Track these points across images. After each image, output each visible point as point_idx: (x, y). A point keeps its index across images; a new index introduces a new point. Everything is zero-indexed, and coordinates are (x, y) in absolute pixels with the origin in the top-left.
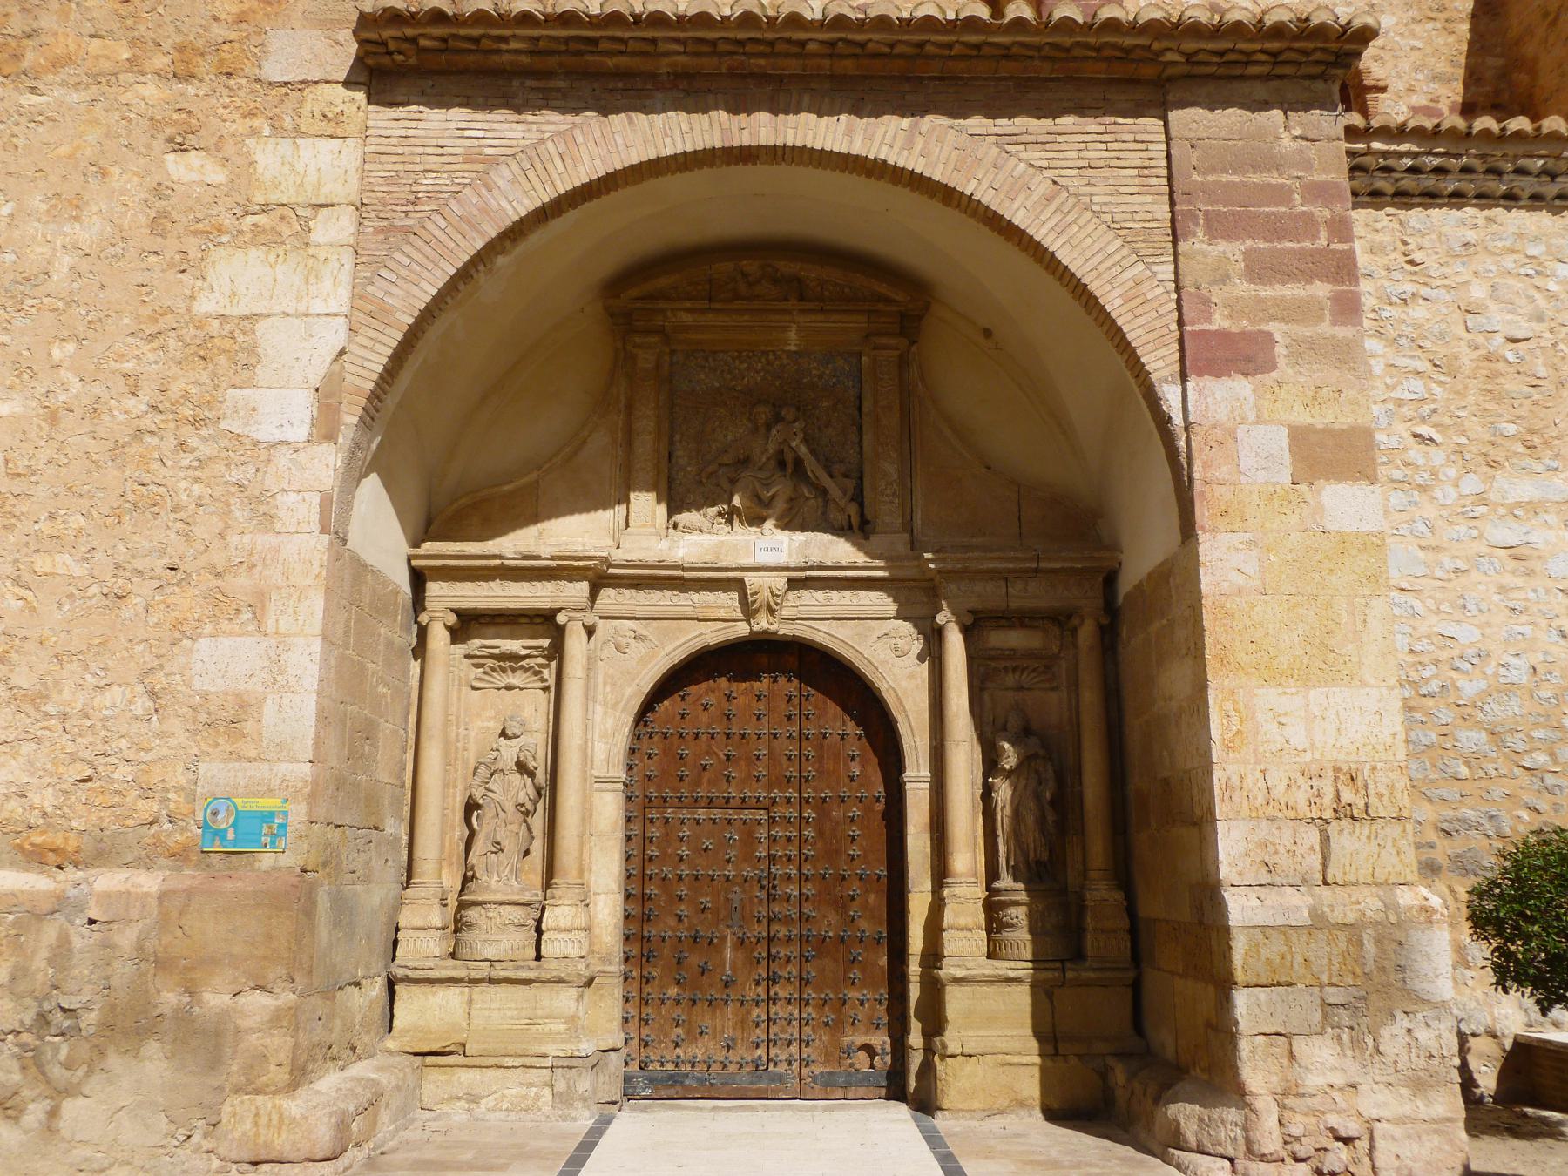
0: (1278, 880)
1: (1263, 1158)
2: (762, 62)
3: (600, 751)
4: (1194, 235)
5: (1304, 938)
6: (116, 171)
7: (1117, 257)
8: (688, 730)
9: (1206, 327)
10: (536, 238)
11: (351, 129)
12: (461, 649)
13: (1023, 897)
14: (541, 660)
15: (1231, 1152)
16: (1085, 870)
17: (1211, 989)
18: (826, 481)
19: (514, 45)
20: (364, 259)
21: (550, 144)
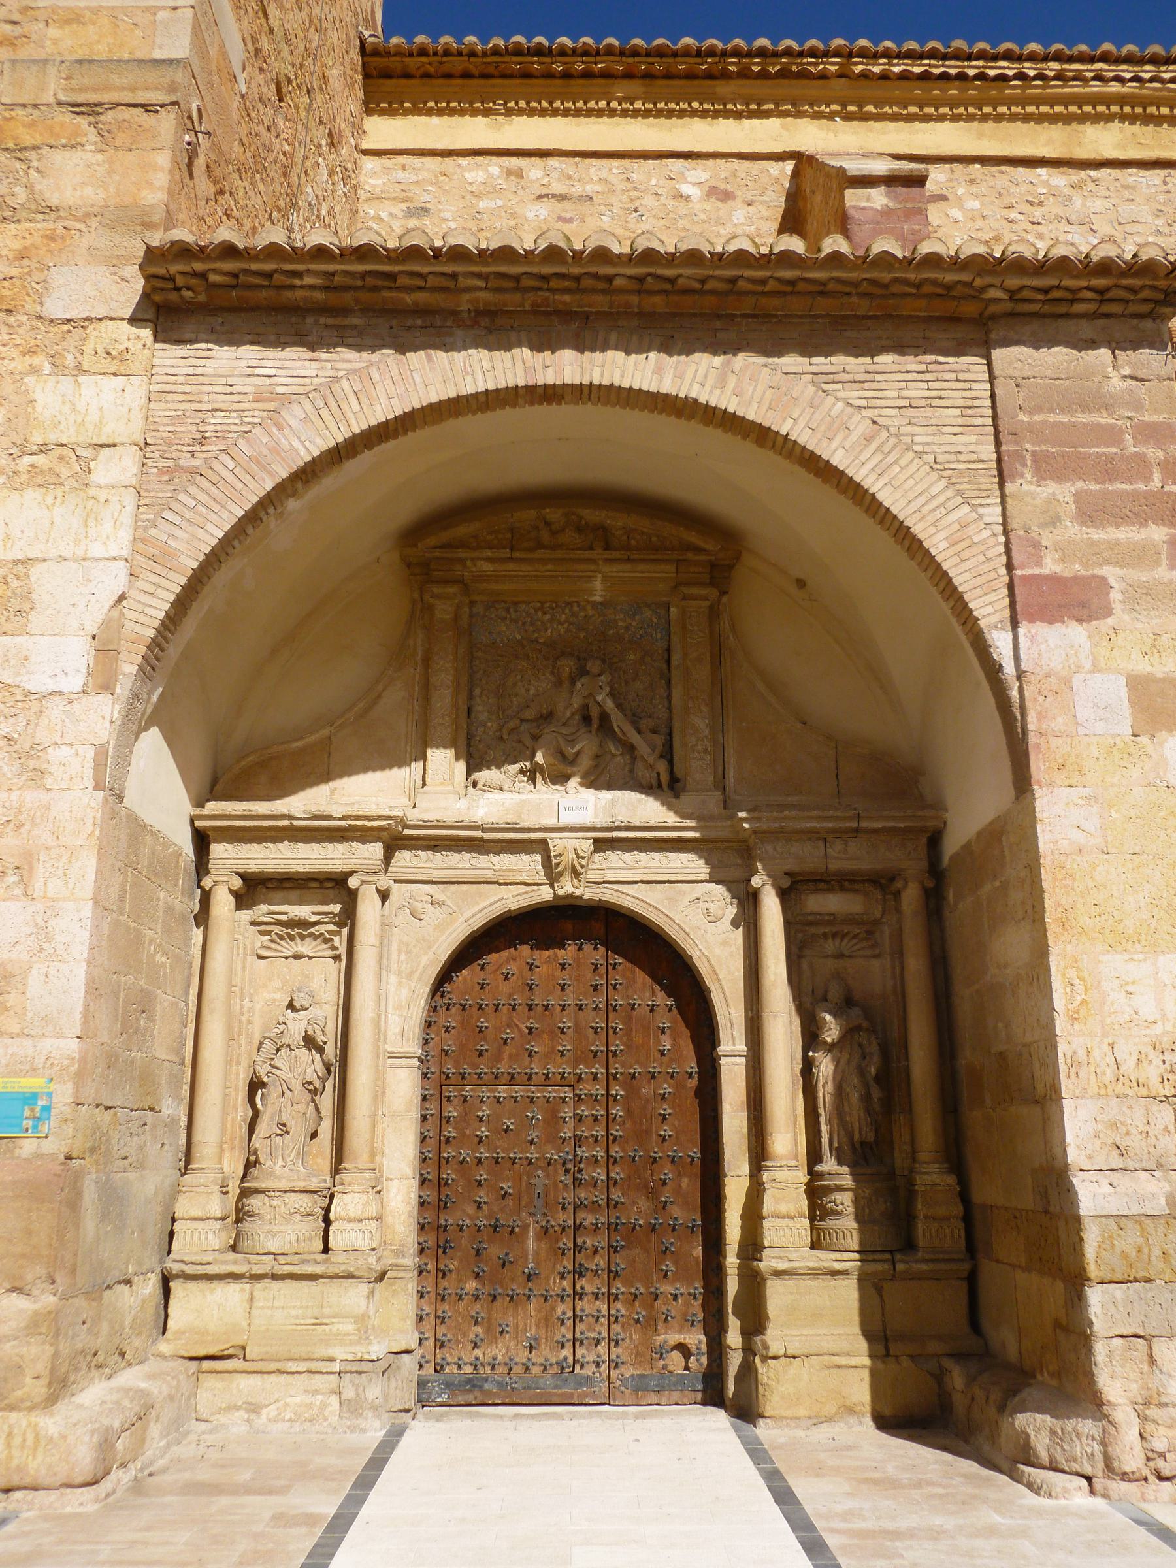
0: (1131, 1165)
1: (1124, 1476)
2: (567, 298)
3: (394, 1024)
4: (1022, 476)
5: (1162, 1229)
7: (941, 499)
8: (487, 1000)
9: (1037, 571)
10: (329, 482)
11: (137, 366)
12: (246, 915)
13: (848, 1181)
14: (331, 927)
15: (1088, 1470)
16: (914, 1152)
17: (1060, 1285)
18: (635, 738)
19: (308, 280)
20: (147, 501)
21: (345, 383)
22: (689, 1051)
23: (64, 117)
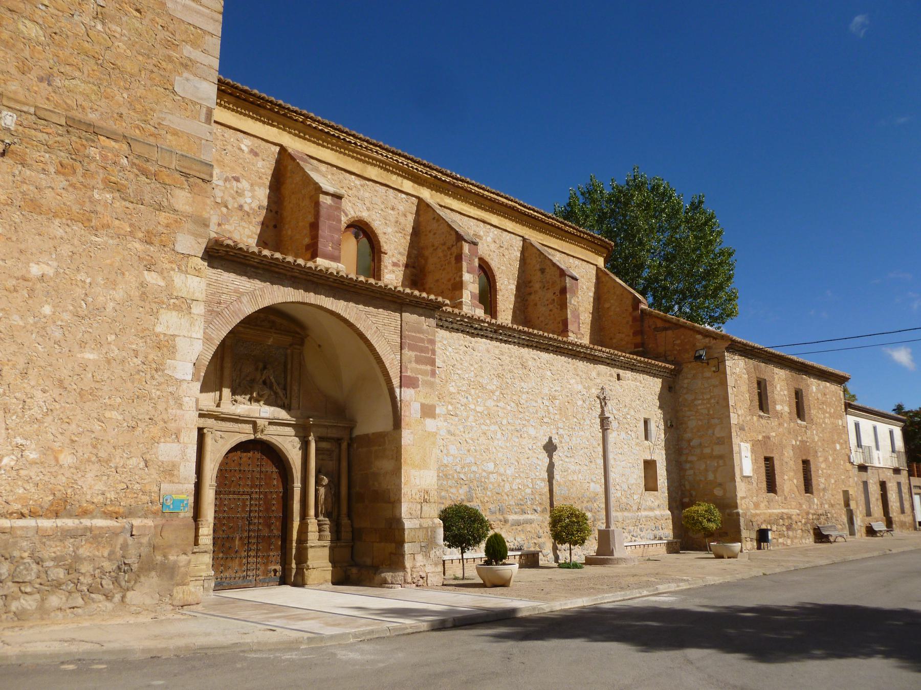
6: (127, 273)
13: (328, 522)
22: (281, 485)
23: (177, 175)
